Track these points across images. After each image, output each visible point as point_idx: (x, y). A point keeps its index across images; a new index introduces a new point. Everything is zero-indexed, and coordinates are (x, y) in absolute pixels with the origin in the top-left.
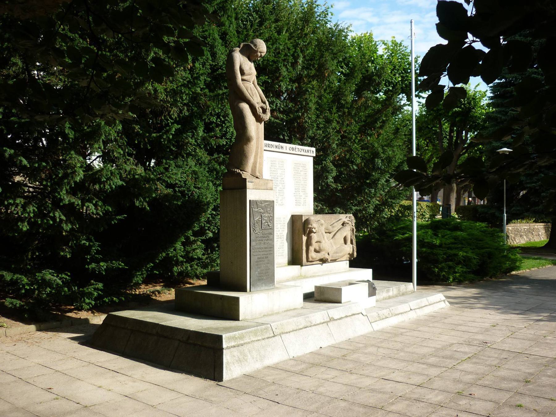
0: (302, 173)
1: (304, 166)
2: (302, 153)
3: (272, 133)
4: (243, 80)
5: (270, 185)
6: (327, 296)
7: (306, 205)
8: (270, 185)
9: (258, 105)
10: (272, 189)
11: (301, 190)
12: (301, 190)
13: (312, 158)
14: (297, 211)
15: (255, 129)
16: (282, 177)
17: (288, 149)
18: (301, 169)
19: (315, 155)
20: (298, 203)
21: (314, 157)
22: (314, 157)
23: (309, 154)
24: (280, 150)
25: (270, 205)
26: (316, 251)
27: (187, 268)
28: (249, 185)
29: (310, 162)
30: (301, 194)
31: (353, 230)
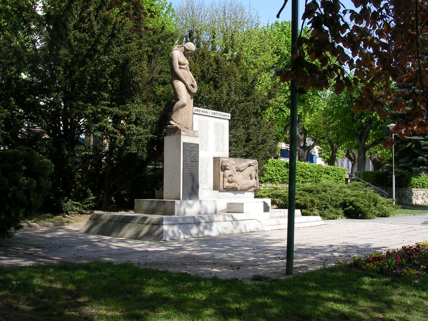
0: (221, 130)
1: (222, 126)
2: (221, 117)
3: (199, 101)
4: (180, 68)
5: (196, 135)
6: (234, 209)
7: (224, 151)
8: (196, 135)
9: (189, 83)
10: (198, 137)
11: (220, 141)
12: (220, 141)
13: (228, 121)
14: (217, 155)
15: (185, 97)
16: (207, 132)
17: (211, 113)
18: (220, 127)
19: (230, 118)
20: (217, 150)
21: (229, 120)
22: (229, 120)
23: (226, 117)
24: (206, 114)
25: (196, 147)
26: (229, 182)
27: (110, 29)
28: (182, 133)
29: (226, 124)
30: (220, 144)
31: (257, 170)
